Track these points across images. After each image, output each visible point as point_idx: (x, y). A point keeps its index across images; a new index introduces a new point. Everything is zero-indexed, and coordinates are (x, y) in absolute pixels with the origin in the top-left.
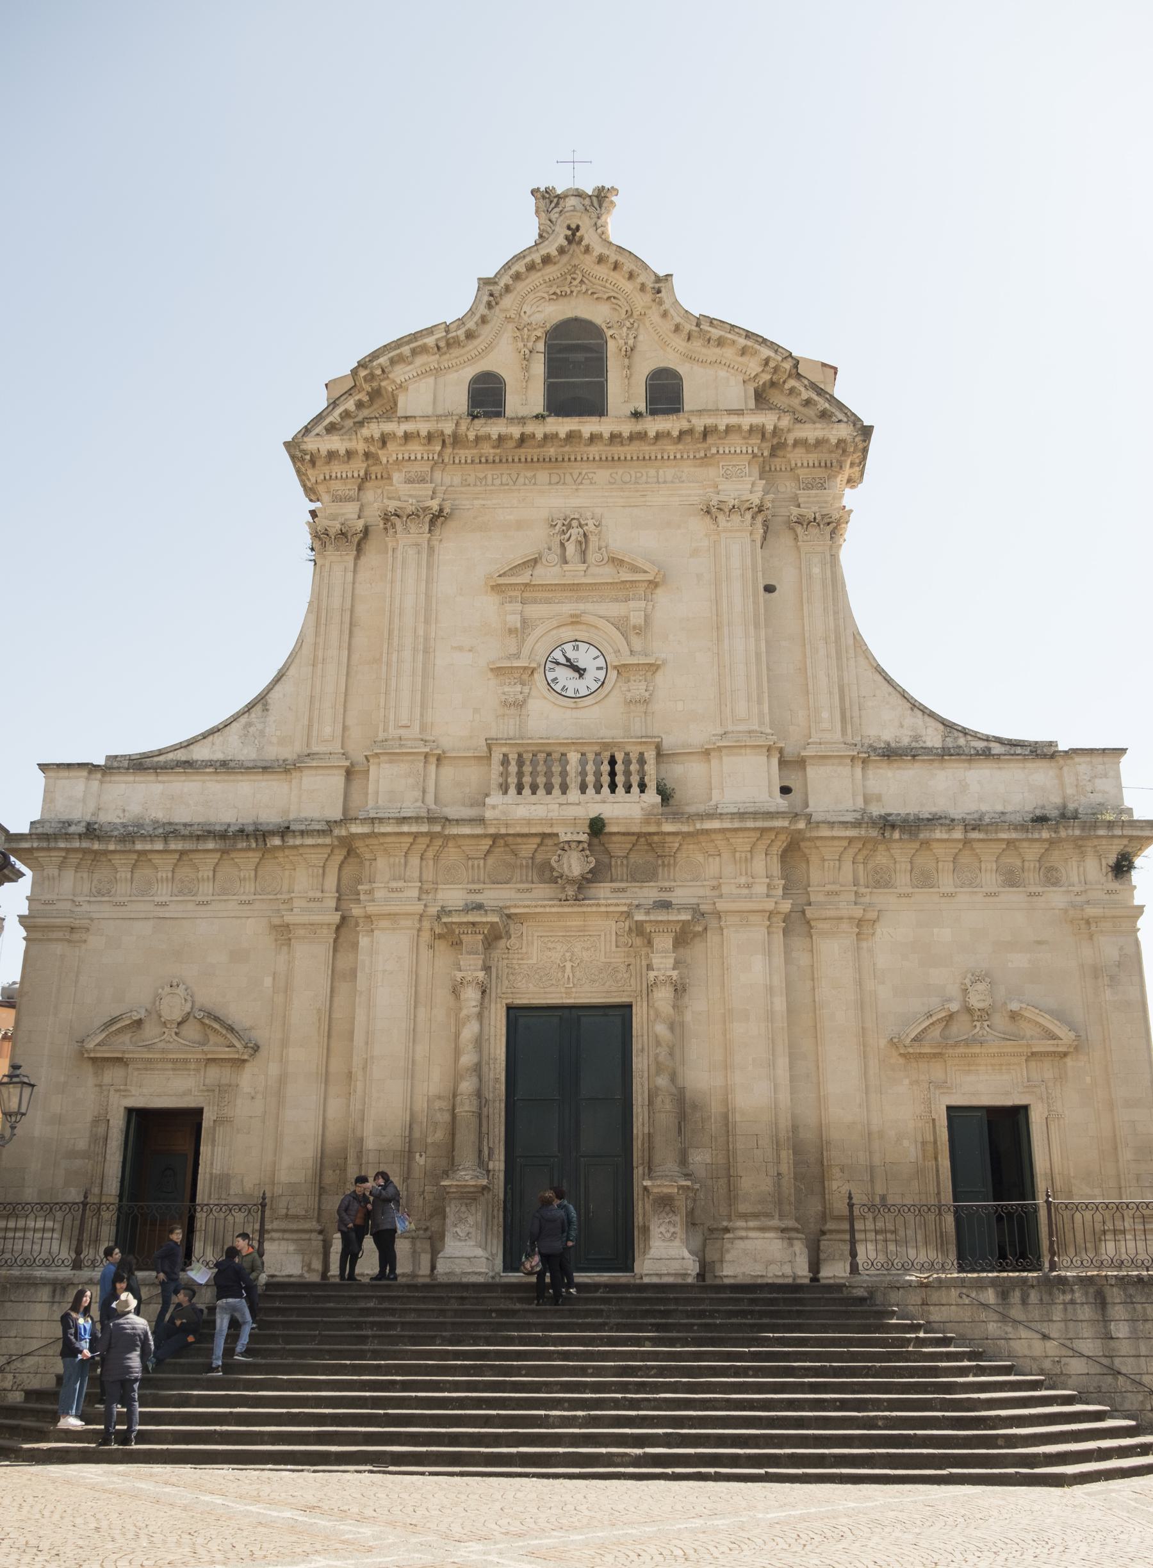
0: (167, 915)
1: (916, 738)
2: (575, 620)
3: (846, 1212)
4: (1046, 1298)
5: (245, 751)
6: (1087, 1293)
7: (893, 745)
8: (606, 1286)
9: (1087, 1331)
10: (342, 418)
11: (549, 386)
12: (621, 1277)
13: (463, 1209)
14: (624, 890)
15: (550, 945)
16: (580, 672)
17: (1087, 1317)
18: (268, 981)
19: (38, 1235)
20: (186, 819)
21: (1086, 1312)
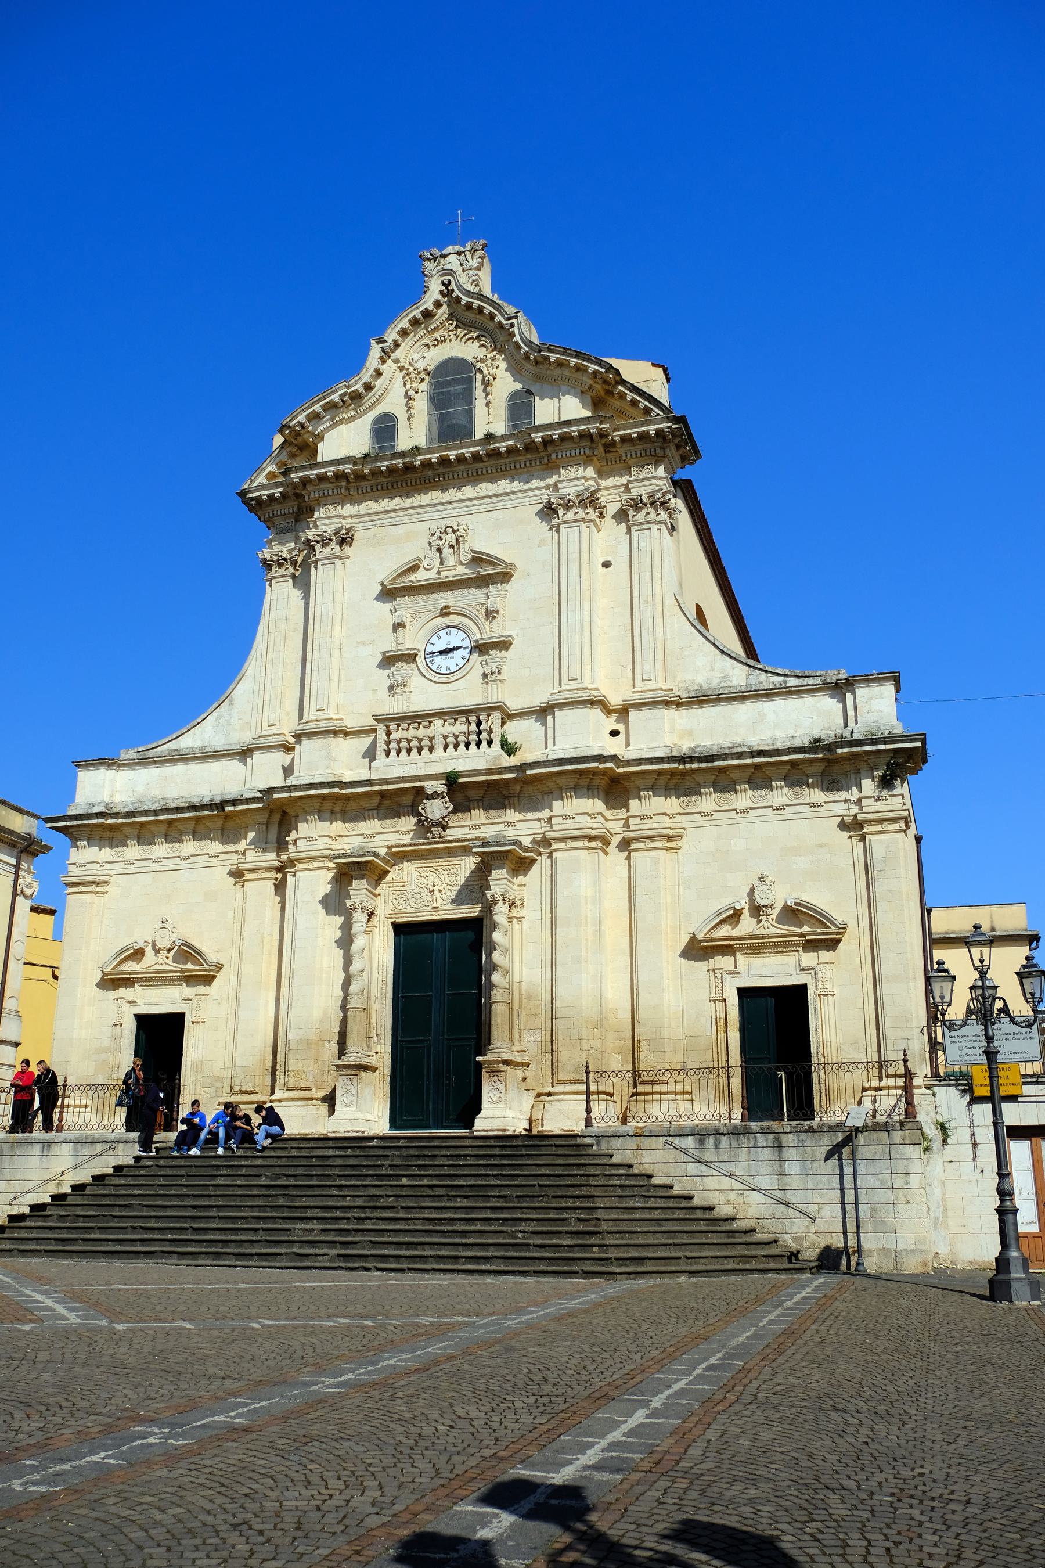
1: (724, 679)
2: (445, 612)
4: (734, 1144)
5: (217, 738)
6: (767, 1139)
7: (705, 687)
8: (405, 1138)
9: (766, 1169)
12: (464, 1132)
13: (349, 1083)
15: (423, 875)
17: (767, 1158)
18: (230, 914)
19: (77, 1110)
20: (175, 795)
21: (766, 1154)
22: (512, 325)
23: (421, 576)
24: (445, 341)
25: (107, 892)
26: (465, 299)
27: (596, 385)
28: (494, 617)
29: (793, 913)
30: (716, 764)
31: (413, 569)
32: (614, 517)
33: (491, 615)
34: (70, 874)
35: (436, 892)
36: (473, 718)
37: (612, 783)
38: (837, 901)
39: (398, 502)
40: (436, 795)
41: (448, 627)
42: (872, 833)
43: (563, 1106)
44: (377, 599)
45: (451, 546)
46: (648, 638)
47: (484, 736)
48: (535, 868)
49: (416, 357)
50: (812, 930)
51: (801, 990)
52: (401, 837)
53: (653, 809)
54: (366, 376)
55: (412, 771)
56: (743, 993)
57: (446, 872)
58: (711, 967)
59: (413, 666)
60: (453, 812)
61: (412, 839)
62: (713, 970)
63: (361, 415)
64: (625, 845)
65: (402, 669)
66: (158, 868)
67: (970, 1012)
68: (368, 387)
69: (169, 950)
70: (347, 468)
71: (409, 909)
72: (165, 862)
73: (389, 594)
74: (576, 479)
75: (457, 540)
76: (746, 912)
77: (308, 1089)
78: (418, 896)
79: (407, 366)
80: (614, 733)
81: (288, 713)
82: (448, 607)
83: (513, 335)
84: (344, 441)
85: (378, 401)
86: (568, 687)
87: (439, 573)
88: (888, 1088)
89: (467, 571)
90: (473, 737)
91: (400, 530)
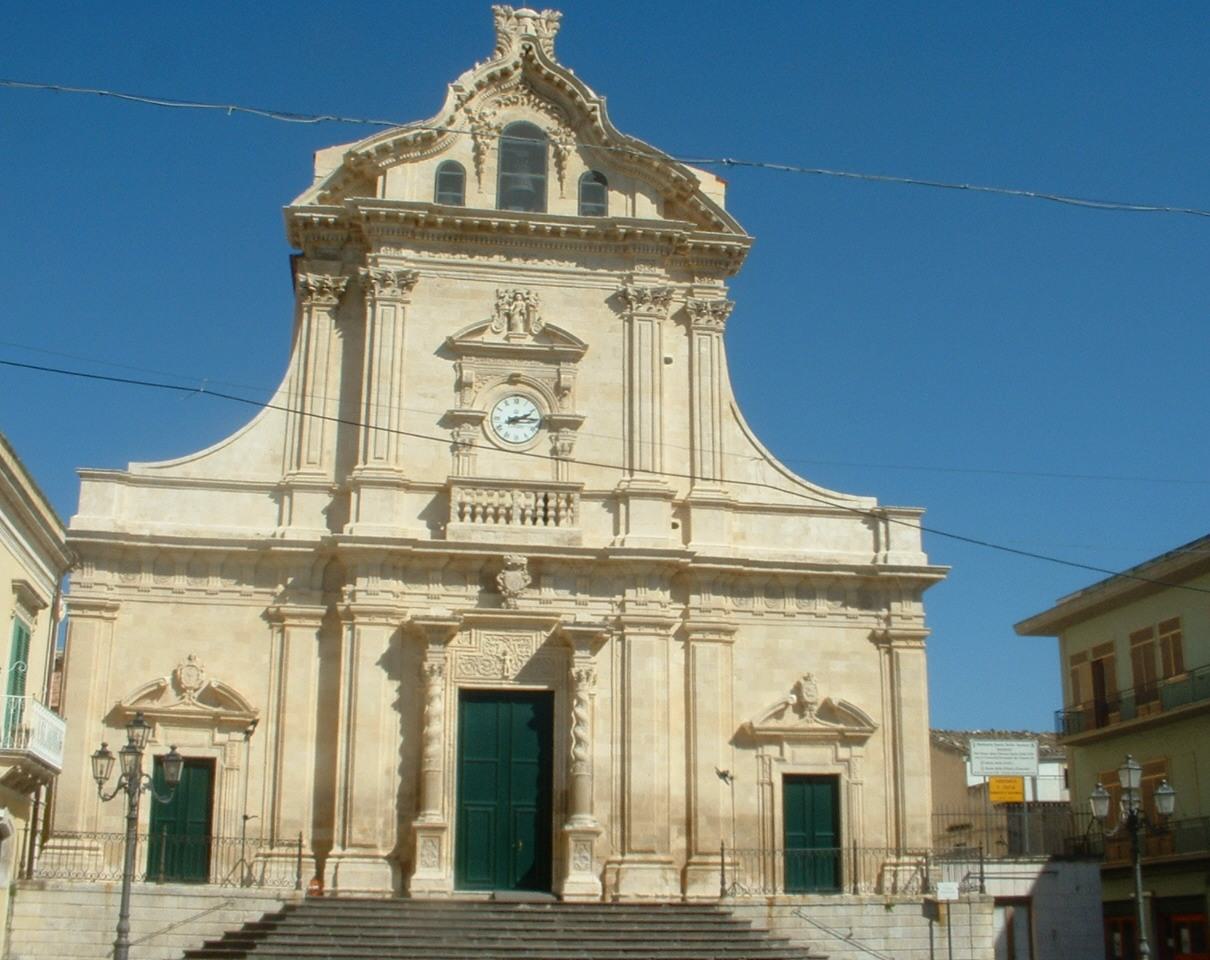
0: (184, 600)
3: (720, 851)
10: (693, 248)
11: (502, 180)
14: (585, 603)
16: (513, 421)
22: (594, 109)
23: (488, 338)
24: (516, 103)
25: (115, 619)
26: (546, 70)
27: (672, 189)
28: (565, 395)
29: (212, 696)
30: (835, 573)
31: (481, 331)
32: (672, 318)
33: (561, 391)
34: (72, 594)
35: (508, 662)
36: (541, 494)
37: (679, 576)
38: (252, 689)
39: (464, 258)
40: (515, 567)
41: (516, 395)
42: (899, 647)
43: (638, 874)
44: (435, 353)
45: (521, 314)
46: (707, 441)
47: (551, 513)
48: (606, 648)
49: (488, 111)
50: (225, 710)
51: (832, 781)
52: (467, 602)
53: (710, 606)
54: (439, 121)
55: (491, 540)
56: (789, 779)
57: (516, 643)
58: (760, 753)
59: (479, 428)
60: (529, 586)
61: (477, 606)
62: (762, 757)
63: (427, 157)
64: (683, 635)
65: (467, 432)
66: (177, 599)
67: (121, 786)
68: (441, 132)
69: (195, 690)
70: (422, 214)
71: (478, 675)
72: (153, 592)
73: (451, 350)
74: (650, 278)
75: (527, 308)
76: (170, 687)
77: (373, 846)
78: (487, 663)
79: (477, 118)
80: (675, 526)
81: (329, 452)
82: (519, 375)
83: (594, 119)
84: (408, 184)
85: (447, 147)
86: (374, 466)
87: (507, 338)
88: (279, 855)
89: (534, 343)
90: (541, 512)
91: (466, 286)
